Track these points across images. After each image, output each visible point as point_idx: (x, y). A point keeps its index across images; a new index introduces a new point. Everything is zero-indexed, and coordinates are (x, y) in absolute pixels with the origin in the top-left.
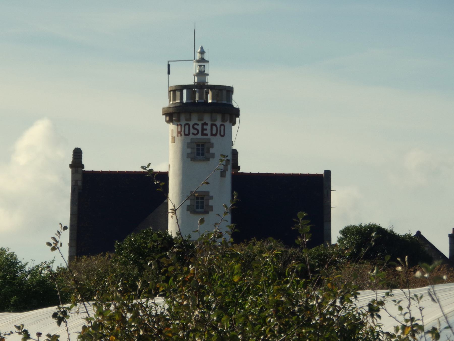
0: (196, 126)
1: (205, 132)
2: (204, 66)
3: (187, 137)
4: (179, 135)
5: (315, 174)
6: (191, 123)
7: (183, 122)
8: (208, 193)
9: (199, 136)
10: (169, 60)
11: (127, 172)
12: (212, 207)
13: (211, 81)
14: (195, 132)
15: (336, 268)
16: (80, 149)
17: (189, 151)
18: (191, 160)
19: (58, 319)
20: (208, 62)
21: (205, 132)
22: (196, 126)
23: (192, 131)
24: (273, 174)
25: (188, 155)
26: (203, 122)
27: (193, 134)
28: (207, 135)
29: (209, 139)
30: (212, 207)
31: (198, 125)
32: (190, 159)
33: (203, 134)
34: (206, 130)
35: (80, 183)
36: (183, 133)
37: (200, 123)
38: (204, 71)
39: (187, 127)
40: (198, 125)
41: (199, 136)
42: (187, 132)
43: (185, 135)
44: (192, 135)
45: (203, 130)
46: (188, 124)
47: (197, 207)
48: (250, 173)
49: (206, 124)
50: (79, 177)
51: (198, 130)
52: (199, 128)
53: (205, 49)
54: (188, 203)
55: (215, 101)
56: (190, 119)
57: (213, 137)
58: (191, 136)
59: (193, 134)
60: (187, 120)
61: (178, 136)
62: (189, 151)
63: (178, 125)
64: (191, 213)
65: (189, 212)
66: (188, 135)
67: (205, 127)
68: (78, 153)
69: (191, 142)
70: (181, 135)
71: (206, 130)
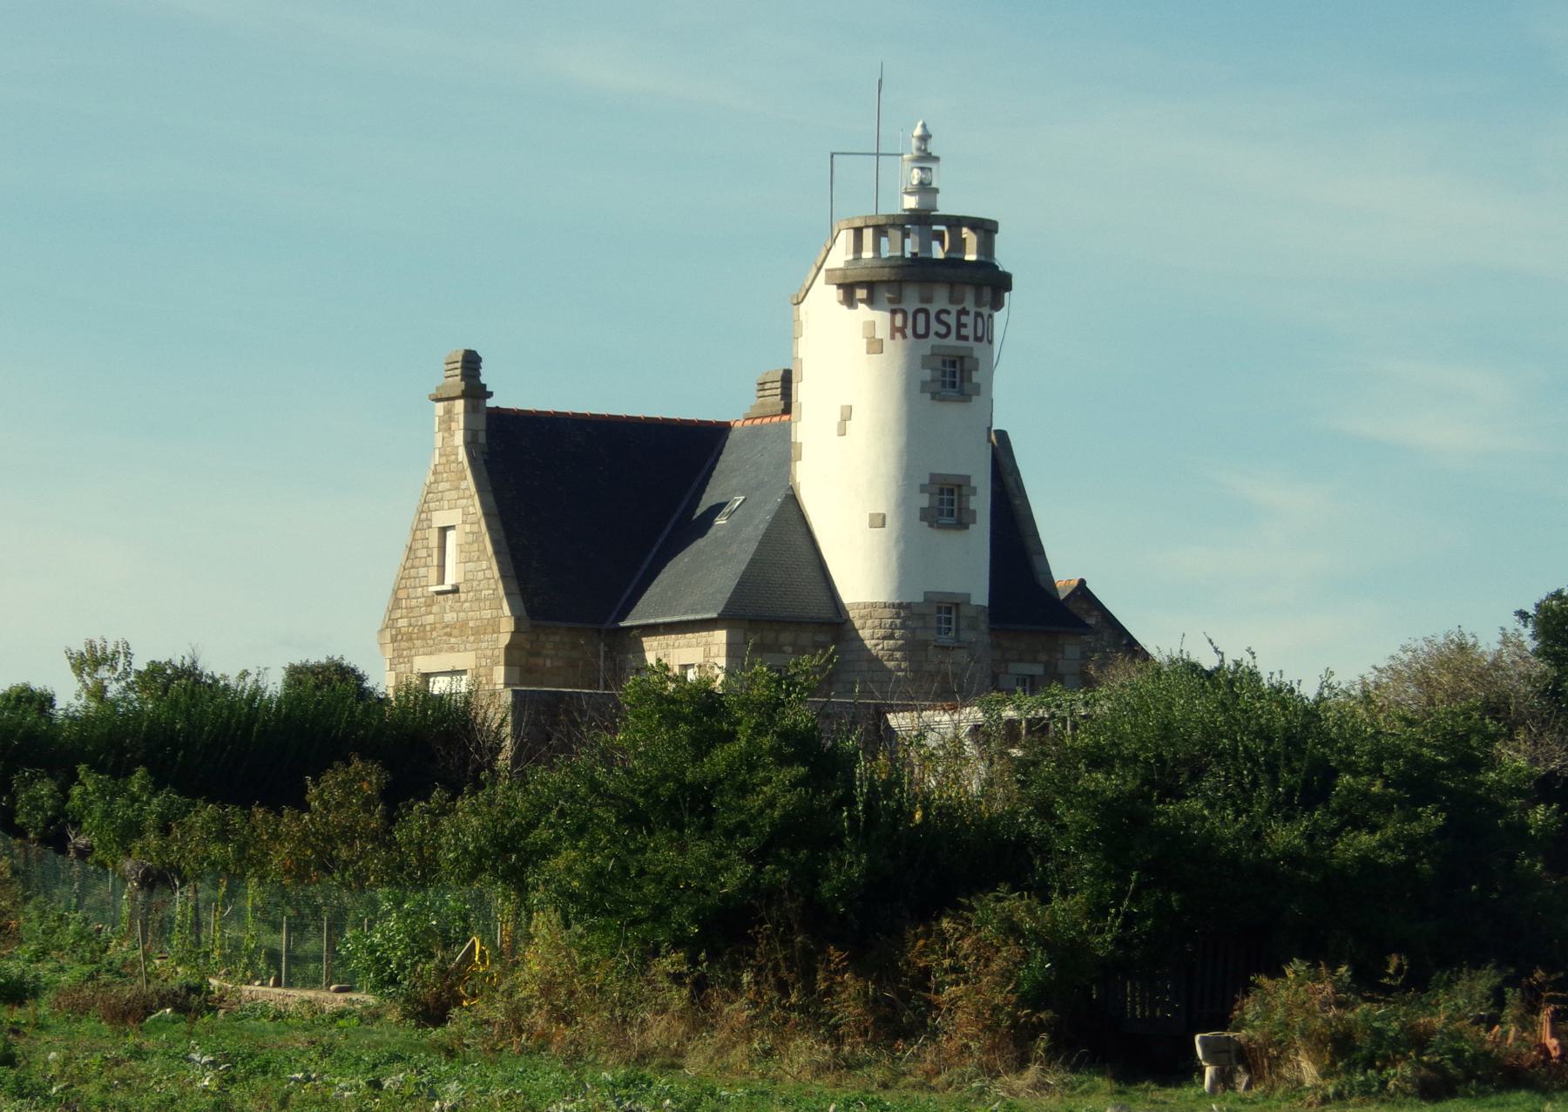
0: (944, 317)
1: (964, 332)
2: (930, 169)
3: (923, 340)
4: (898, 335)
5: (657, 419)
6: (933, 309)
7: (911, 304)
8: (968, 478)
9: (952, 340)
10: (833, 151)
11: (574, 414)
12: (922, 491)
13: (946, 206)
14: (943, 330)
15: (903, 645)
16: (475, 352)
17: (927, 375)
18: (933, 398)
19: (80, 723)
20: (936, 159)
21: (964, 332)
22: (944, 317)
23: (935, 326)
24: (657, 419)
25: (924, 387)
26: (959, 307)
27: (937, 334)
28: (966, 338)
29: (972, 349)
30: (922, 491)
31: (948, 312)
32: (929, 395)
33: (960, 337)
34: (965, 326)
35: (482, 438)
36: (909, 331)
37: (954, 309)
38: (930, 184)
39: (921, 318)
40: (948, 312)
41: (952, 340)
42: (921, 330)
43: (915, 335)
44: (935, 337)
45: (960, 325)
46: (926, 312)
47: (941, 513)
48: (497, 407)
49: (964, 312)
50: (481, 423)
51: (948, 327)
52: (951, 320)
53: (930, 130)
54: (924, 501)
55: (983, 259)
56: (929, 300)
57: (977, 343)
58: (933, 340)
59: (937, 334)
60: (923, 300)
61: (893, 337)
62: (927, 375)
63: (894, 312)
64: (931, 526)
65: (926, 524)
66: (926, 335)
67: (964, 319)
68: (471, 363)
69: (932, 354)
70: (904, 336)
71: (965, 326)
